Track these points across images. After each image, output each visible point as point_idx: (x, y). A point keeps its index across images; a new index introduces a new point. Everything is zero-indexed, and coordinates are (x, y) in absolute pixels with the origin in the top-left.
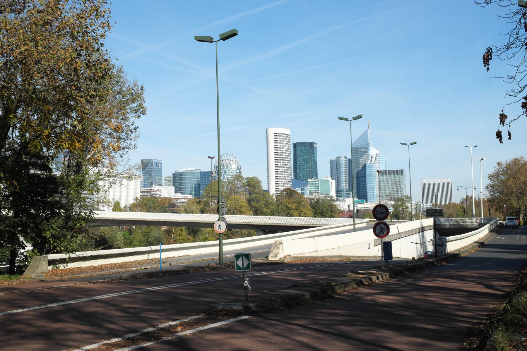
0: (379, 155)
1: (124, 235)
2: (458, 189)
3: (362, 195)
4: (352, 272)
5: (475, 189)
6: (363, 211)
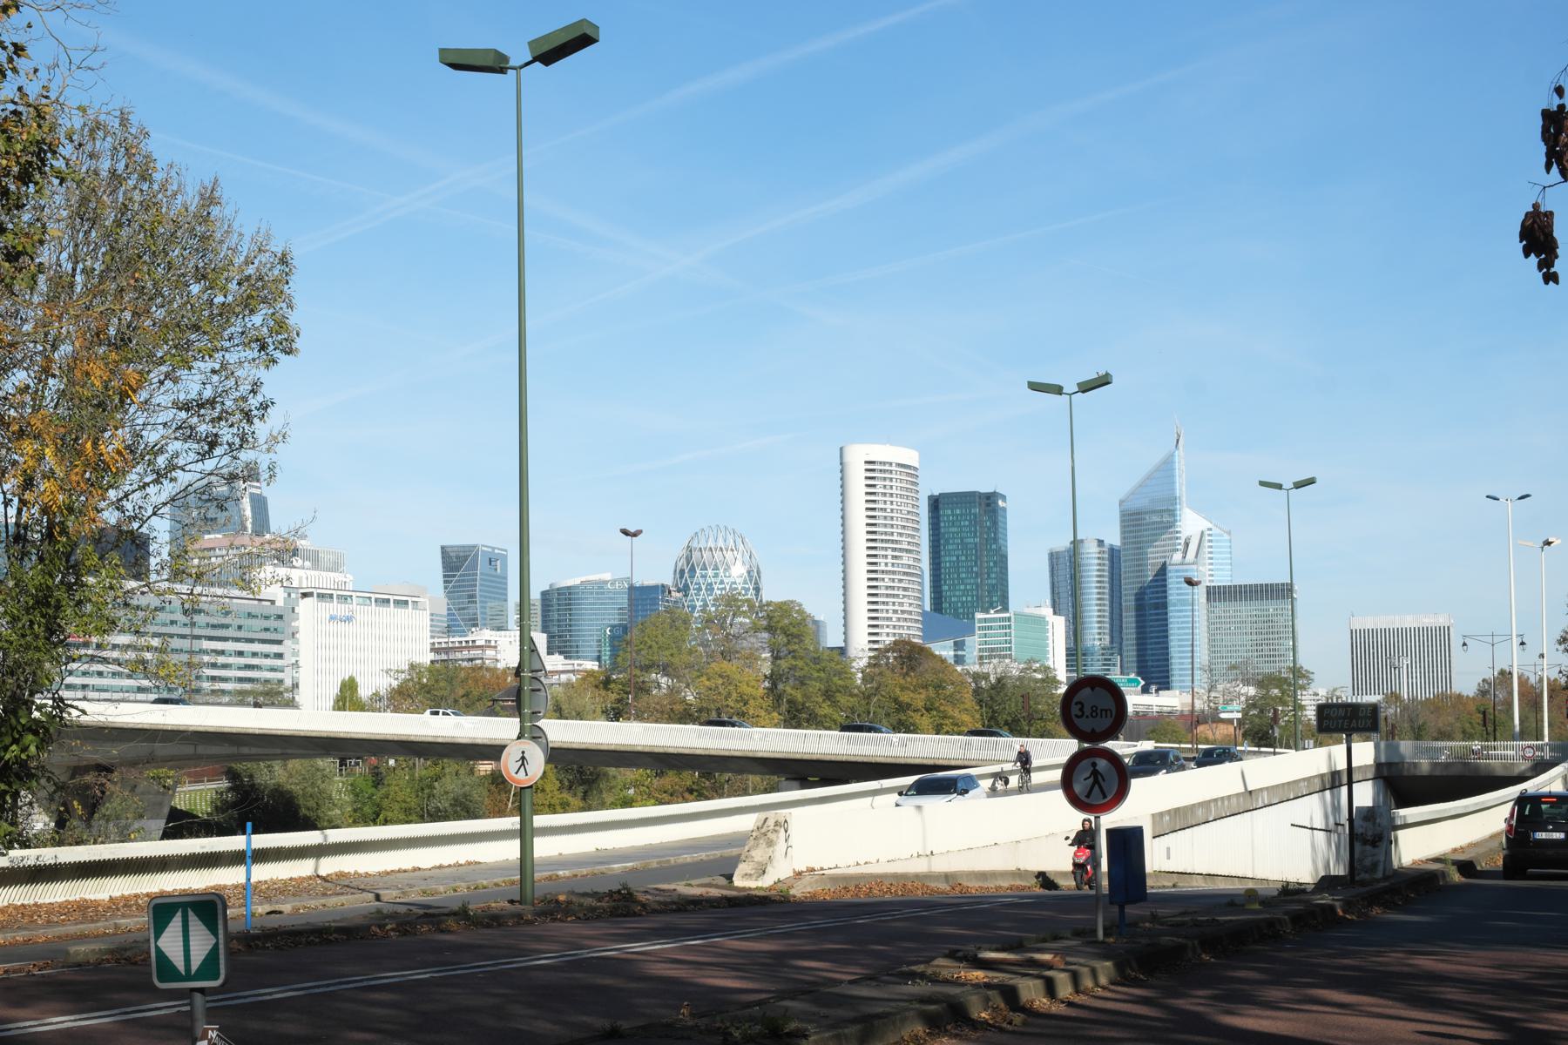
0: (1209, 535)
1: (356, 792)
2: (1464, 644)
3: (1152, 666)
4: (952, 955)
5: (1523, 644)
6: (1154, 718)
